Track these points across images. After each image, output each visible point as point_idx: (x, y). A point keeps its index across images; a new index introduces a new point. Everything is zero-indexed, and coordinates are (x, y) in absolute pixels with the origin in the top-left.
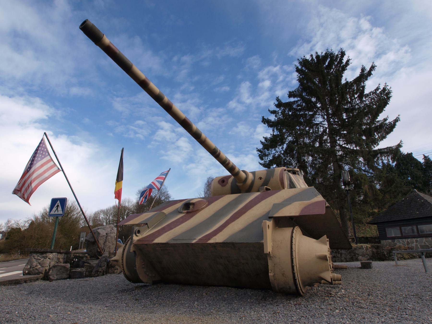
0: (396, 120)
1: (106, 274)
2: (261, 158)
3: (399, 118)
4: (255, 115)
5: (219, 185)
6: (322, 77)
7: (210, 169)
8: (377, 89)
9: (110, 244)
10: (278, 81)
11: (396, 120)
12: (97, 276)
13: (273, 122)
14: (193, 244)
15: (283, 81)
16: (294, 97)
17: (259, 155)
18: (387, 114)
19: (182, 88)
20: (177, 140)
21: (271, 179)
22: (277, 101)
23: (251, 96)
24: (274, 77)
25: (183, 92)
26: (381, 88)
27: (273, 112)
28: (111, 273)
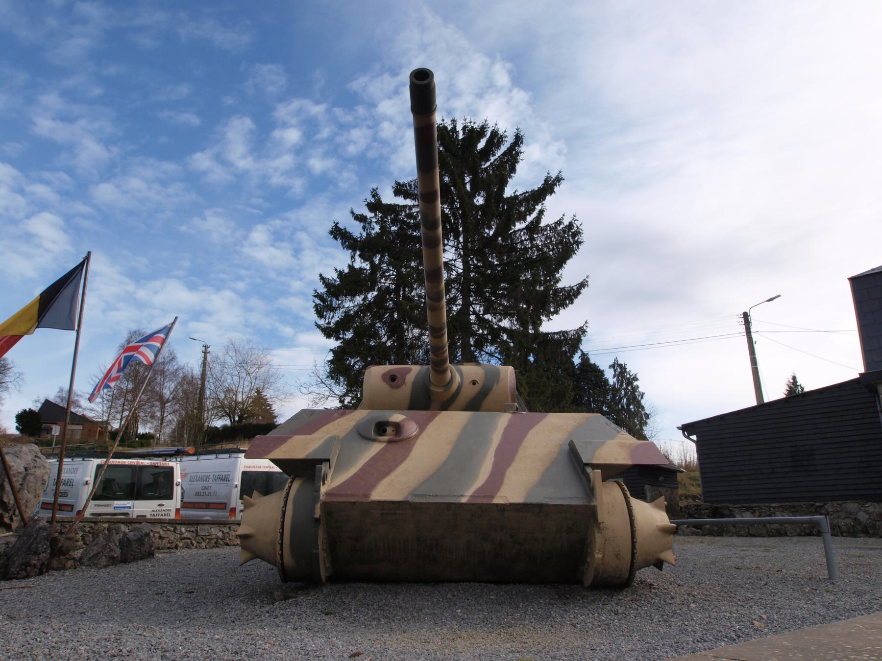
0: (582, 285)
1: (47, 571)
2: (320, 313)
4: (254, 201)
5: (384, 384)
6: (464, 169)
7: (117, 309)
8: (559, 223)
9: (30, 496)
10: (319, 136)
11: (582, 285)
12: (24, 578)
13: (355, 240)
14: (462, 504)
15: (330, 140)
16: (405, 198)
17: (316, 306)
18: (568, 275)
19: (68, 83)
20: (28, 217)
21: (495, 387)
22: (374, 196)
23: (251, 152)
24: (310, 126)
25: (69, 95)
26: (566, 222)
27: (361, 218)
28: (58, 569)
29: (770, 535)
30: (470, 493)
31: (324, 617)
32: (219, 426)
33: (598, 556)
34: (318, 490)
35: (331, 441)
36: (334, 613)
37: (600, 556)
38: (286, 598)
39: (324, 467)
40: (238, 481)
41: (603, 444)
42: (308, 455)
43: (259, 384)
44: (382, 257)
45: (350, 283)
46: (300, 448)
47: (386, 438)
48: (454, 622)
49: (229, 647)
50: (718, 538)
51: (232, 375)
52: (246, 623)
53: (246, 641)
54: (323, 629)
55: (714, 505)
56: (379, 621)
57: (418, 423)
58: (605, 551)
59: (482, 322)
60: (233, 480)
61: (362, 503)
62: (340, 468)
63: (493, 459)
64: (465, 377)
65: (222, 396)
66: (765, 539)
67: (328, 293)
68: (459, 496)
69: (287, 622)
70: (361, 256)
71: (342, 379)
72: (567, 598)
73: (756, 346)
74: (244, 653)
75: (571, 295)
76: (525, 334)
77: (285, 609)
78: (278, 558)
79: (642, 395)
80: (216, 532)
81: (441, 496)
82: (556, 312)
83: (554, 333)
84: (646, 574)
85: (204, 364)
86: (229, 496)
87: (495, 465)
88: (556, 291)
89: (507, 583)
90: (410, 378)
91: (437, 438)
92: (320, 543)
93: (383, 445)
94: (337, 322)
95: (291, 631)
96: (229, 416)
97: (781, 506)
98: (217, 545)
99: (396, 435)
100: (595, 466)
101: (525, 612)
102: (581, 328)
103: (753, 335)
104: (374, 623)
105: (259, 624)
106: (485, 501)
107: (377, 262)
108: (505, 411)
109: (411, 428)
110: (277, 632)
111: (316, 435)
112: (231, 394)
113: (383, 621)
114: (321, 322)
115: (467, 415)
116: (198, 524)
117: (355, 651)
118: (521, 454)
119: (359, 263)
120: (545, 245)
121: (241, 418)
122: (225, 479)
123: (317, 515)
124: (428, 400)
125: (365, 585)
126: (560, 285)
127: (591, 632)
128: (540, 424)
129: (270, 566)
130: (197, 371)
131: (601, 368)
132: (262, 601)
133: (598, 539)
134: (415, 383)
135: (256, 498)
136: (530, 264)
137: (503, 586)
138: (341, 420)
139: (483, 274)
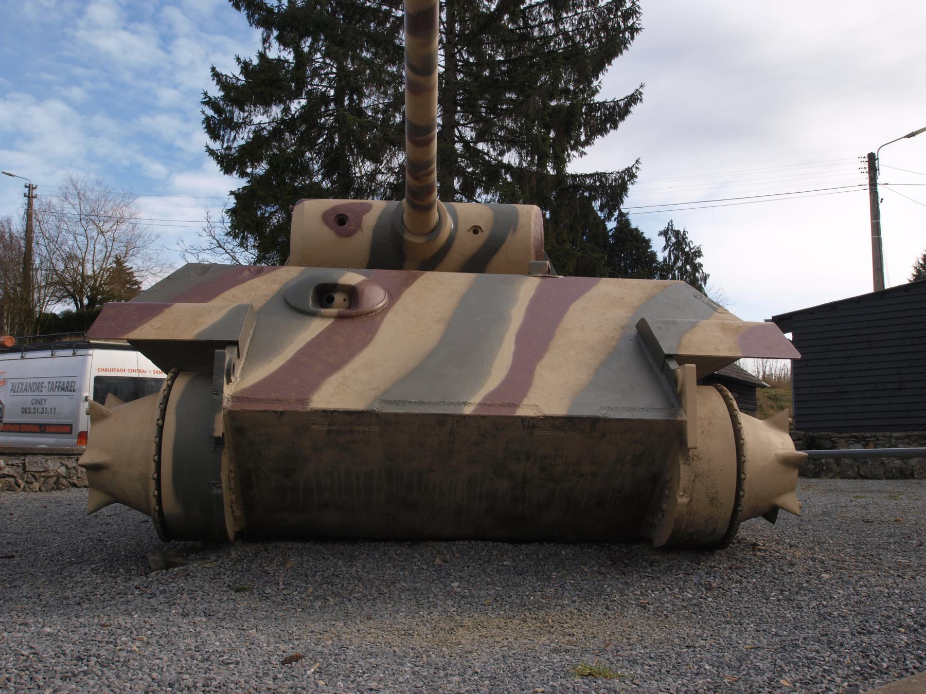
0: (633, 99)
2: (213, 130)
3: (641, 93)
5: (326, 229)
11: (633, 99)
13: (270, 11)
14: (464, 417)
17: (207, 120)
21: (509, 238)
29: (890, 475)
30: (477, 398)
31: (234, 595)
32: (57, 313)
33: (683, 500)
34: (220, 392)
35: (239, 313)
36: (250, 589)
37: (685, 500)
38: (168, 565)
39: (229, 354)
40: (88, 391)
41: (694, 325)
42: (200, 334)
43: (118, 249)
44: (315, 40)
45: (262, 83)
46: (185, 322)
47: (333, 311)
48: (450, 602)
49: (68, 648)
50: (814, 481)
51: (75, 235)
52: (100, 605)
53: (99, 638)
54: (232, 615)
55: (811, 434)
56: (326, 600)
57: (387, 290)
58: (693, 492)
59: (472, 153)
60: (80, 390)
61: (297, 412)
62: (258, 355)
63: (513, 348)
64: (460, 220)
65: (61, 266)
66: (883, 481)
67: (226, 98)
68: (459, 404)
69: (171, 604)
70: (278, 38)
71: (251, 241)
72: (626, 565)
73: (882, 207)
74: (94, 659)
75: (614, 114)
76: (542, 177)
77: (167, 583)
78: (153, 501)
79: (705, 278)
80: (55, 466)
81: (429, 403)
82: (588, 142)
83: (586, 176)
84: (752, 529)
85: (29, 214)
86: (75, 415)
87: (517, 355)
88: (592, 108)
89: (528, 541)
90: (370, 220)
91: (417, 315)
92: (224, 477)
93: (328, 322)
94: (242, 148)
95: (178, 620)
96: (73, 297)
97: (907, 437)
98: (57, 486)
99: (349, 307)
100: (683, 360)
101: (562, 586)
102: (629, 170)
103: (879, 188)
104: (318, 604)
105: (123, 608)
106: (504, 412)
107: (306, 50)
108: (529, 274)
109: (376, 297)
110: (153, 620)
111: (216, 303)
112: (75, 264)
113: (332, 601)
114: (216, 146)
115: (466, 278)
116: (25, 454)
117: (291, 653)
118: (559, 340)
119: (275, 52)
120: (578, 31)
121: (92, 300)
122: (69, 388)
123: (219, 433)
124: (399, 254)
125: (299, 545)
126: (598, 98)
127: (673, 617)
128: (587, 294)
129: (142, 516)
130: (18, 226)
131: (647, 236)
132: (128, 571)
133: (685, 473)
134: (377, 229)
135: (112, 404)
136: (551, 61)
137: (523, 546)
138: (256, 282)
139: (477, 77)
